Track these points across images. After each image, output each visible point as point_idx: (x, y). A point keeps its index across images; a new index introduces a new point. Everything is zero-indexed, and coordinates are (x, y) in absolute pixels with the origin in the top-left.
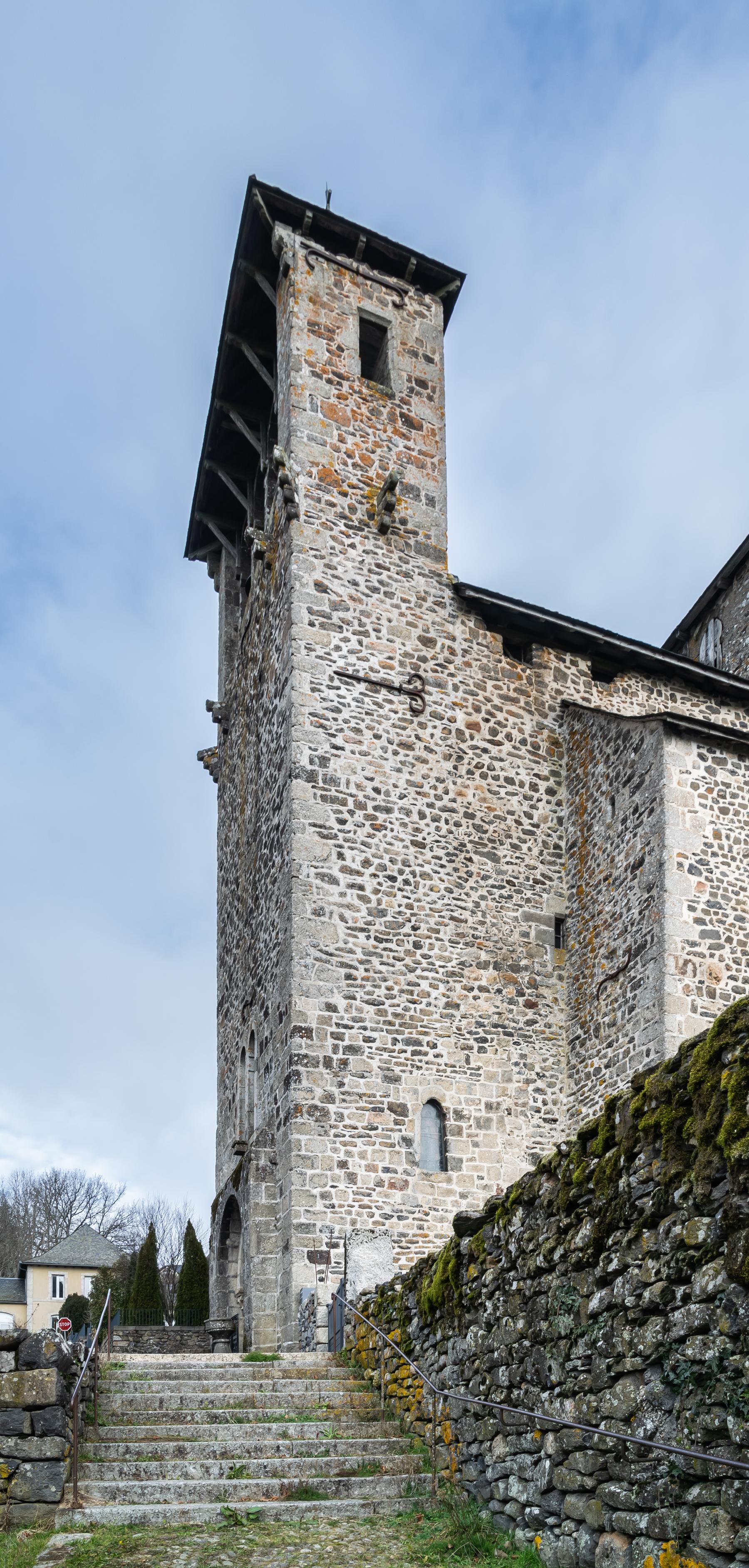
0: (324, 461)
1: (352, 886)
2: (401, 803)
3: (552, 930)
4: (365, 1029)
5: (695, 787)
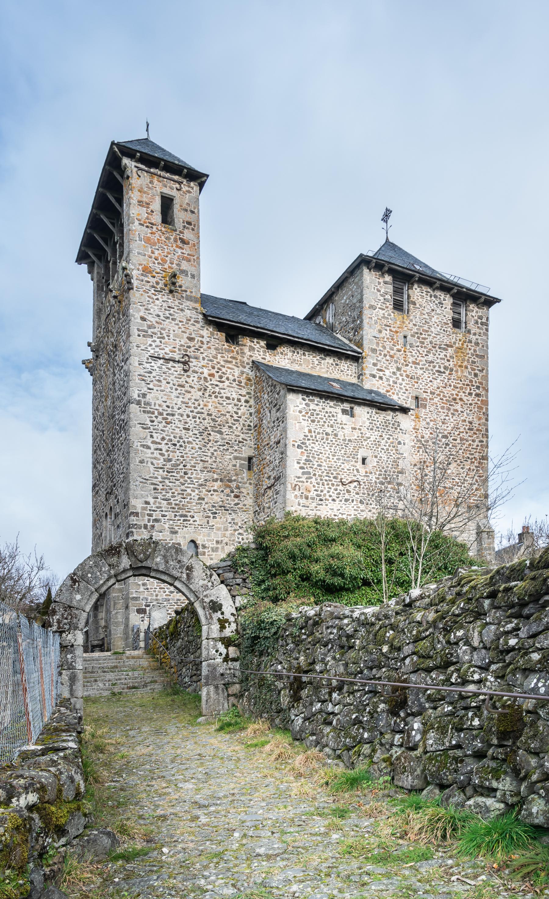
0: (145, 263)
1: (157, 449)
2: (179, 411)
3: (247, 463)
4: (162, 511)
5: (300, 412)
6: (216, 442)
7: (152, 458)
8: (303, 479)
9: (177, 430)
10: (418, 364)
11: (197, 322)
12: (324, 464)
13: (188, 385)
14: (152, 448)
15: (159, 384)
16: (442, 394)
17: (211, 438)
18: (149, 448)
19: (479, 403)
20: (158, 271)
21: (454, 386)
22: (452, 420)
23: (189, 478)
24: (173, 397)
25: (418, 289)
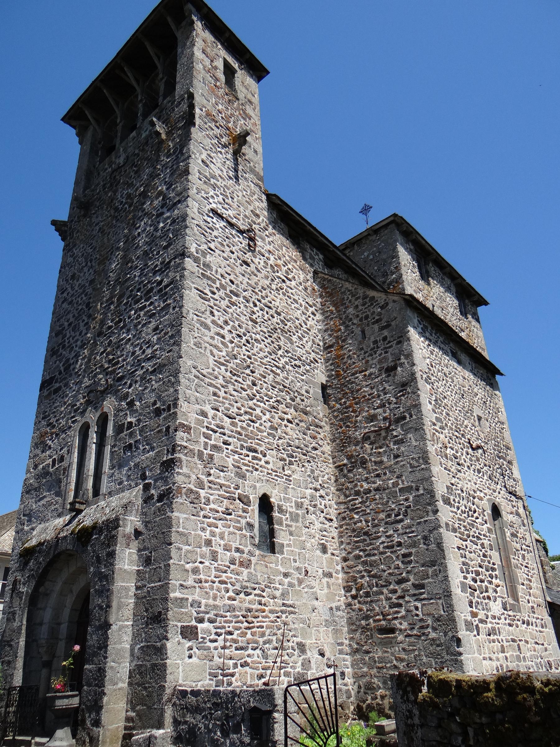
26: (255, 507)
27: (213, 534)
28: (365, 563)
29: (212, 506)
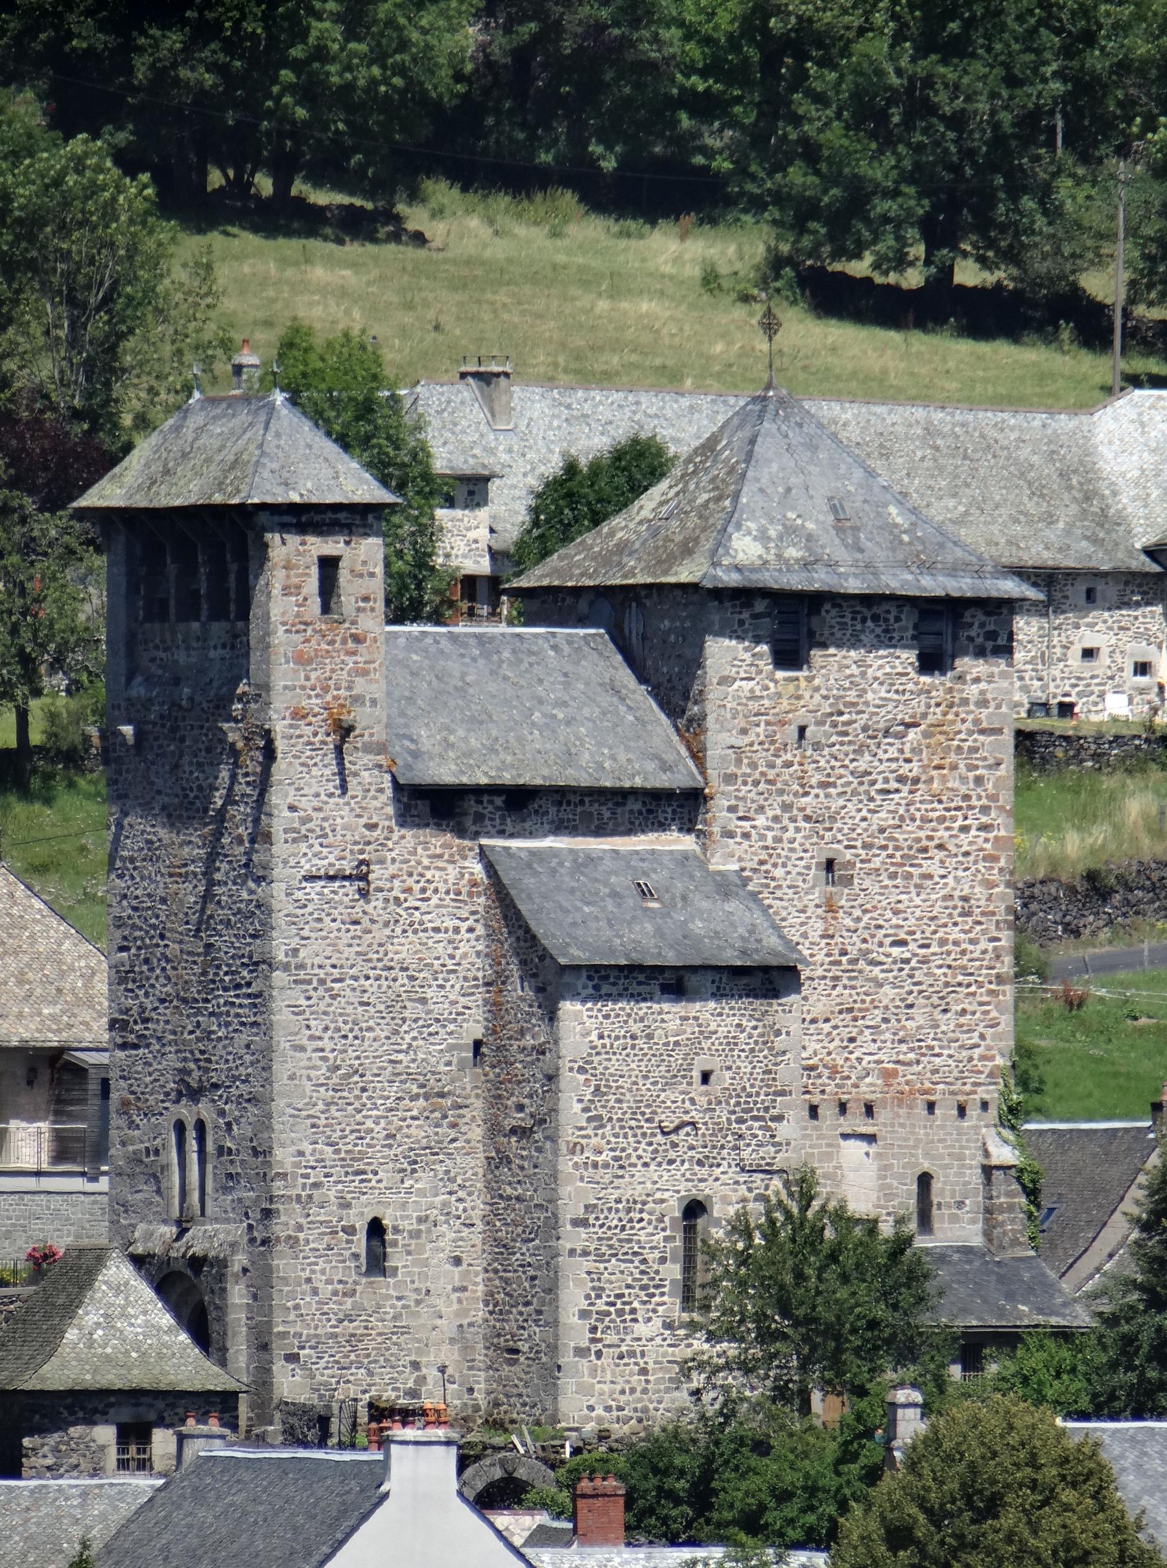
6: (416, 1020)
7: (309, 1068)
8: (590, 1132)
9: (349, 1009)
10: (834, 785)
11: (381, 790)
12: (628, 1096)
13: (367, 918)
14: (309, 1049)
15: (319, 926)
16: (891, 844)
17: (407, 1014)
18: (302, 1049)
19: (988, 846)
20: (317, 710)
21: (922, 820)
22: (917, 901)
23: (370, 1098)
24: (341, 948)
25: (834, 612)
26: (361, 1237)
27: (313, 1272)
28: (501, 1278)
29: (312, 1246)
